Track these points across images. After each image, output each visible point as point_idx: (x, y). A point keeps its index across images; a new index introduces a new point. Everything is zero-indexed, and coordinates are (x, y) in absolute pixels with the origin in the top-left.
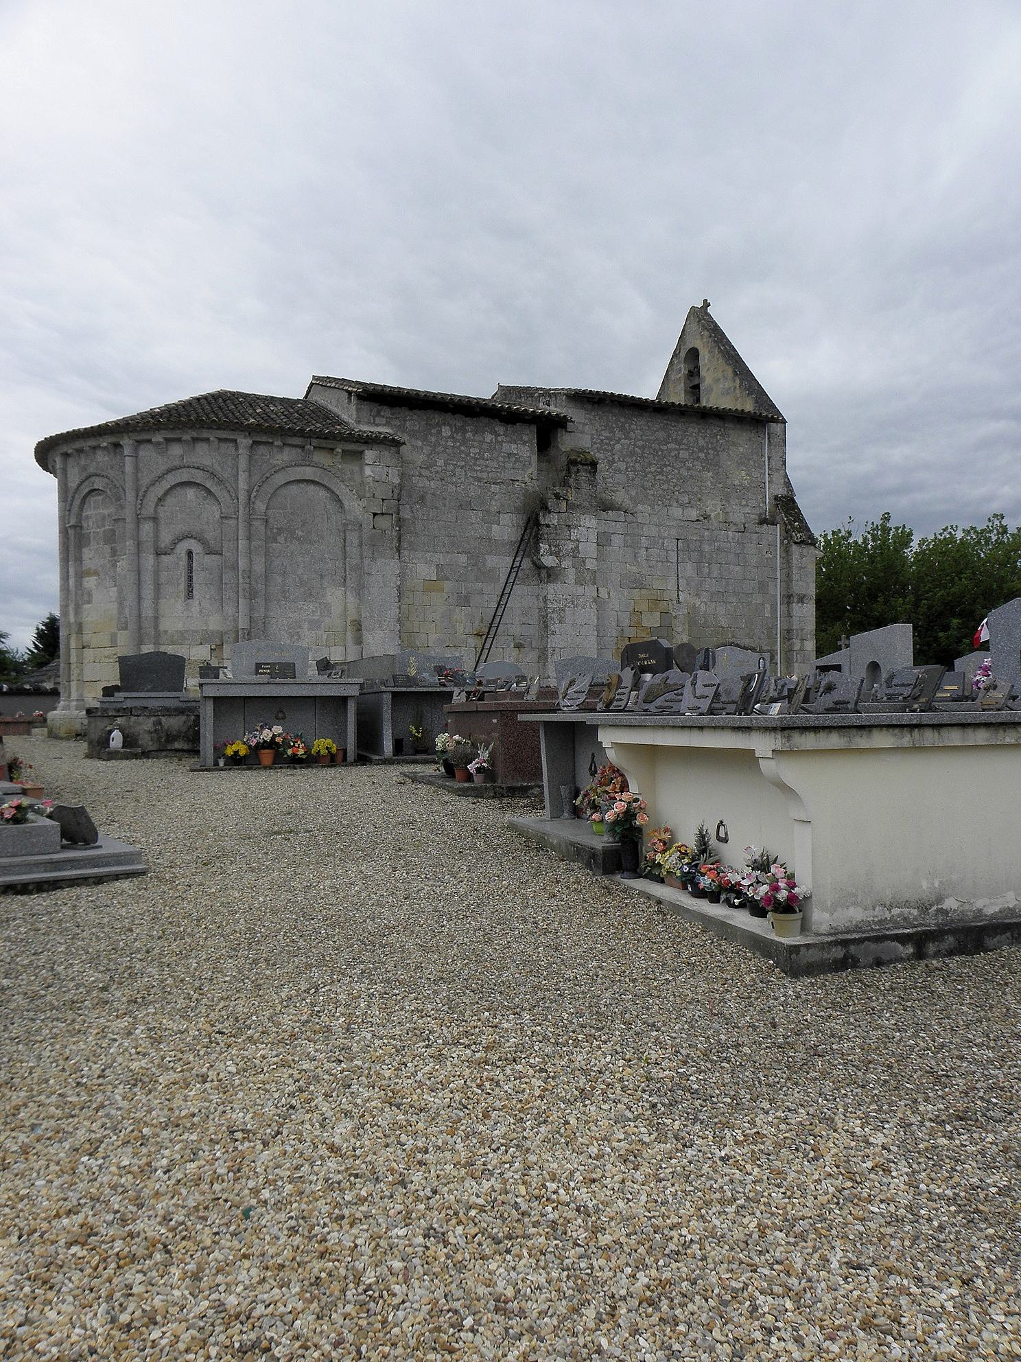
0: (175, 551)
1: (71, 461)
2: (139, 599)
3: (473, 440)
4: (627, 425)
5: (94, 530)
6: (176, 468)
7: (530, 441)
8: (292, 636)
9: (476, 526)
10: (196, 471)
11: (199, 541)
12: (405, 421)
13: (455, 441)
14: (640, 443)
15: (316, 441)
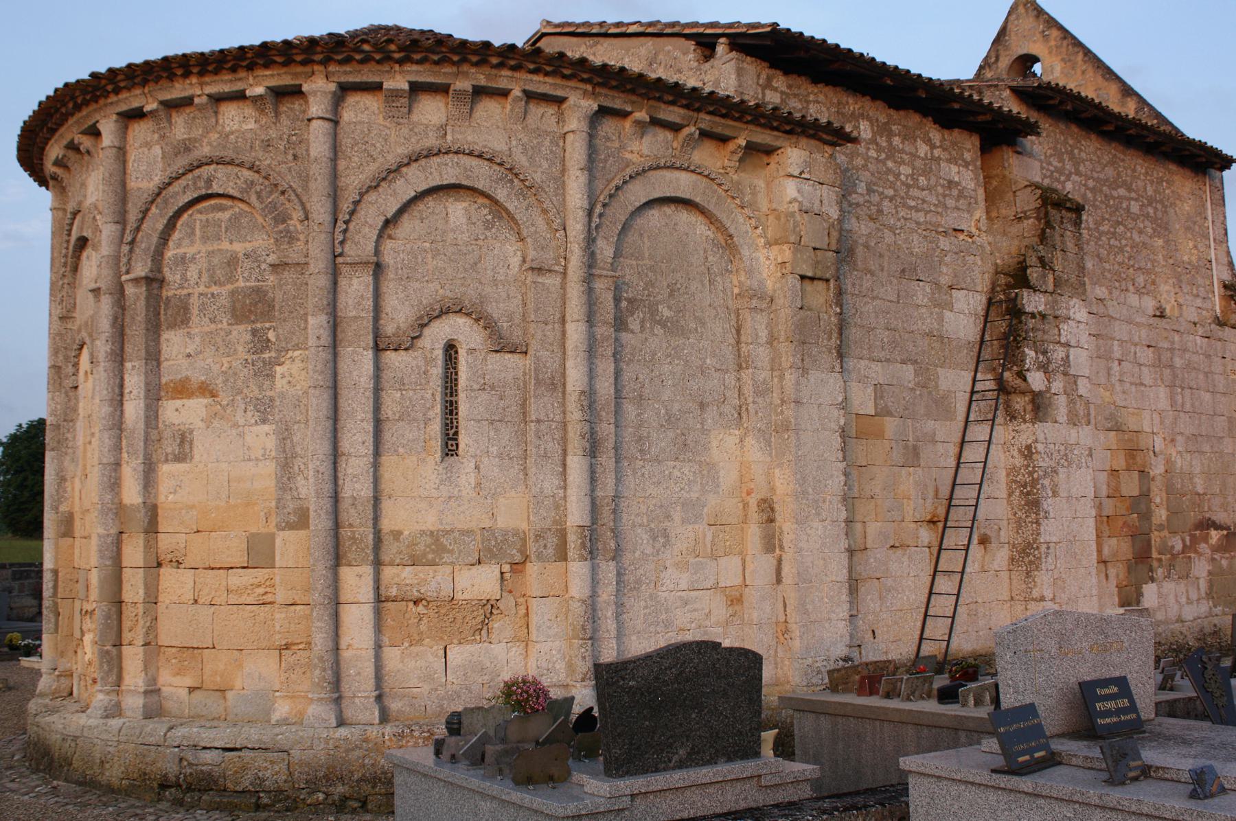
0: (420, 343)
1: (140, 131)
2: (336, 455)
3: (902, 151)
4: (1076, 151)
5: (202, 289)
6: (430, 154)
7: (973, 161)
8: (655, 539)
9: (924, 310)
10: (475, 162)
11: (477, 320)
12: (808, 102)
13: (880, 149)
14: (1091, 183)
15: (708, 117)
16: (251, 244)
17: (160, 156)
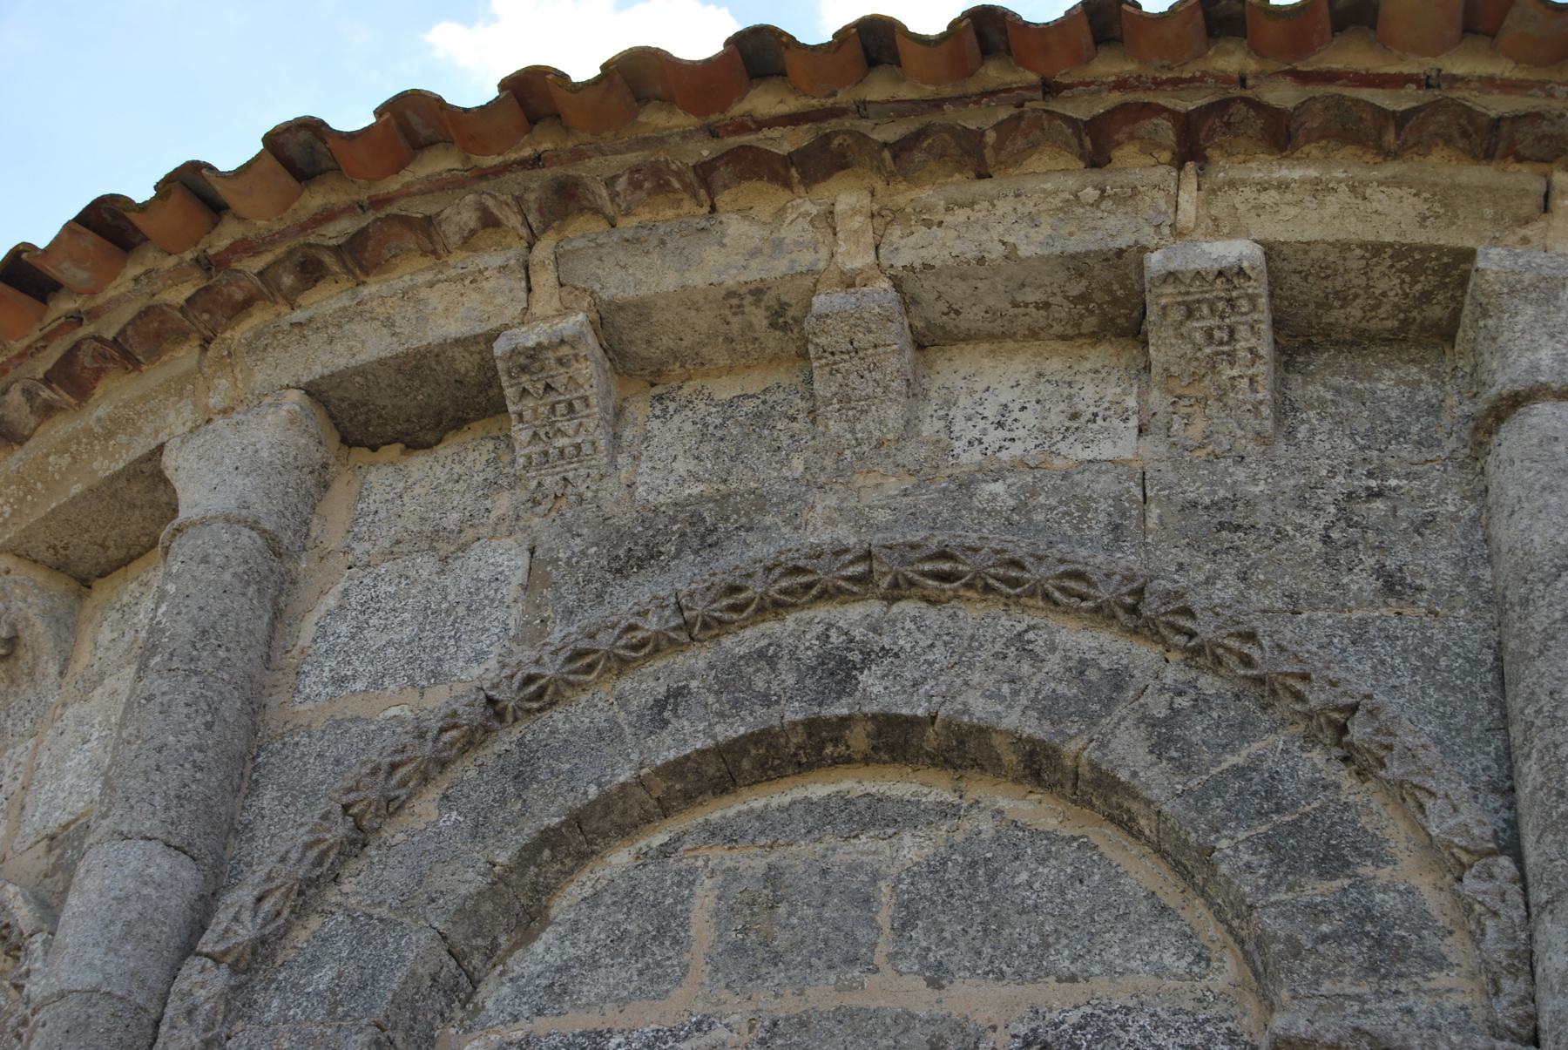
16: (1078, 991)
17: (519, 577)
